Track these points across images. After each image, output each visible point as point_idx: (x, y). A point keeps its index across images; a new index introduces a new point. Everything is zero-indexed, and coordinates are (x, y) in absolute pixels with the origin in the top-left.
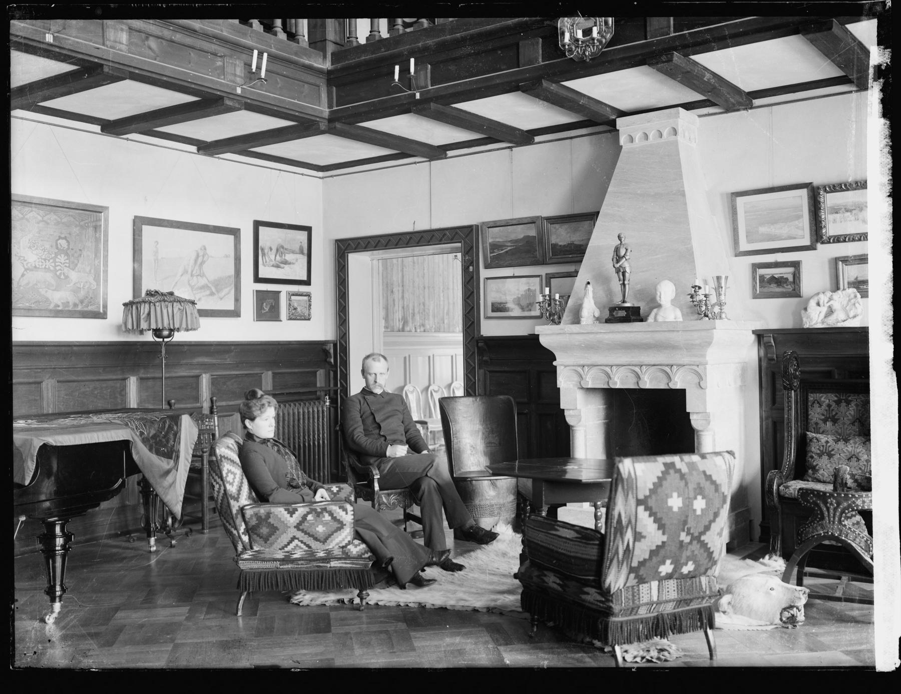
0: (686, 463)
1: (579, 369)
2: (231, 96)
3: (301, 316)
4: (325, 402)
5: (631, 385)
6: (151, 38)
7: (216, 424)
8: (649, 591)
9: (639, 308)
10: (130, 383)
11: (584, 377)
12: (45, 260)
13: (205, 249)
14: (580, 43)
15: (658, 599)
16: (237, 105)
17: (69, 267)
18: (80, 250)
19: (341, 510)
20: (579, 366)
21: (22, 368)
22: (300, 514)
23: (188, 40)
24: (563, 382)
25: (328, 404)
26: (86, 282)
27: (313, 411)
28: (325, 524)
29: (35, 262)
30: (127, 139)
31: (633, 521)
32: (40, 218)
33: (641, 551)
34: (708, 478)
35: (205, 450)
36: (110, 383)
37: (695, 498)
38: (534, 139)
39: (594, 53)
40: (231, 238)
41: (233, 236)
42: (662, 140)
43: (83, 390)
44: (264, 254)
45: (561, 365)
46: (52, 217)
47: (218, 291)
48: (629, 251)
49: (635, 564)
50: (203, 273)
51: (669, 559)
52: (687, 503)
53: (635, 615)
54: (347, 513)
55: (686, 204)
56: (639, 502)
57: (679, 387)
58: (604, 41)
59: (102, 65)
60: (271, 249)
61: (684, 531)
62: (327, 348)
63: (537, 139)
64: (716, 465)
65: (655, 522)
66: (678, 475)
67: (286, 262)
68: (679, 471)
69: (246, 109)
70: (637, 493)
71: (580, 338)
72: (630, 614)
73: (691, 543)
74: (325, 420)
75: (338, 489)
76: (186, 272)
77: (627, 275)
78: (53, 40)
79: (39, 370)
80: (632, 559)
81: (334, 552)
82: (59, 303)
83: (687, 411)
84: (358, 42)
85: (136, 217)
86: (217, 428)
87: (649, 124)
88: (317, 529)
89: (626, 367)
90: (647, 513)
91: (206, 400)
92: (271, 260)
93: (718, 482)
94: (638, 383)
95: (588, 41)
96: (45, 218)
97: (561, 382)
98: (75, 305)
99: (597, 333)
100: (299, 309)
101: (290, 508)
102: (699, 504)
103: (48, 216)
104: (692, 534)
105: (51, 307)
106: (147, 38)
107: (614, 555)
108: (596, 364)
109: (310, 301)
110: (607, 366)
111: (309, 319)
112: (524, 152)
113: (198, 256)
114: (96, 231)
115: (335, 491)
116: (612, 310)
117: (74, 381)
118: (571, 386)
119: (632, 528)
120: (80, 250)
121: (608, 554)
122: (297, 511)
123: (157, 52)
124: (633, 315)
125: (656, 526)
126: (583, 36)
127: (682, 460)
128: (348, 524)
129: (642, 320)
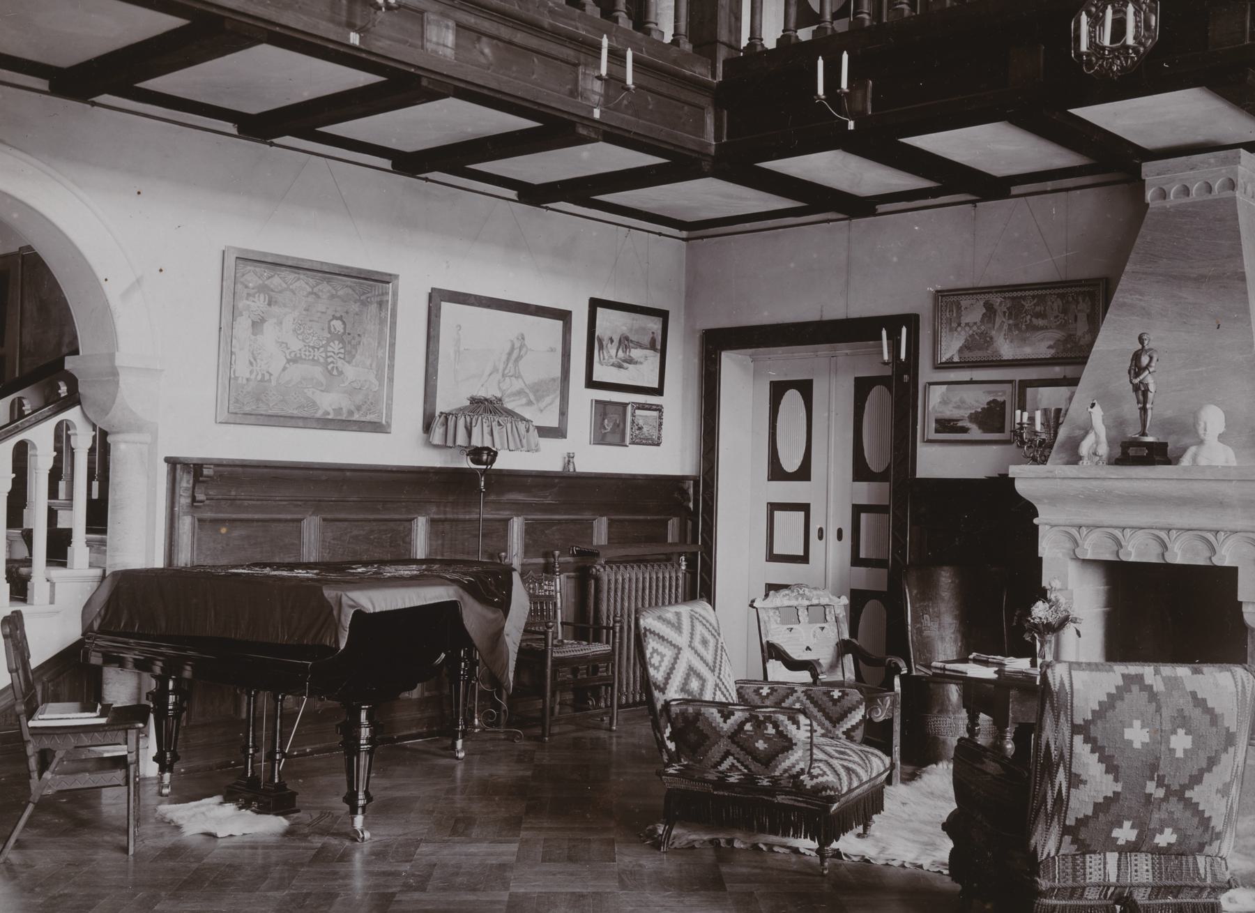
0: (1164, 679)
1: (1074, 531)
2: (586, 122)
3: (647, 439)
4: (680, 565)
5: (1153, 558)
6: (484, 39)
7: (558, 588)
8: (1102, 866)
9: (1166, 444)
10: (417, 526)
11: (1080, 542)
12: (313, 348)
13: (523, 339)
14: (1107, 53)
15: (1118, 880)
16: (593, 135)
17: (344, 359)
18: (359, 335)
19: (790, 722)
20: (1073, 526)
21: (277, 498)
22: (736, 721)
23: (534, 42)
24: (1047, 550)
25: (683, 568)
26: (365, 381)
27: (664, 578)
28: (767, 739)
29: (300, 350)
30: (427, 179)
31: (1067, 756)
32: (310, 290)
33: (1081, 804)
34: (1199, 702)
35: (551, 624)
36: (392, 524)
37: (1174, 732)
38: (1010, 191)
39: (1126, 67)
40: (559, 324)
41: (561, 322)
42: (1210, 197)
43: (355, 532)
44: (601, 347)
45: (1046, 524)
46: (325, 288)
47: (538, 401)
48: (1155, 359)
49: (1070, 822)
50: (519, 373)
51: (1128, 820)
52: (1159, 738)
53: (1079, 899)
54: (798, 728)
55: (1246, 293)
56: (1076, 729)
57: (1227, 563)
58: (1142, 49)
59: (419, 76)
60: (612, 340)
61: (1152, 779)
62: (686, 486)
63: (1015, 190)
64: (1217, 685)
65: (1100, 760)
66: (1145, 695)
67: (631, 361)
68: (1149, 688)
69: (606, 141)
70: (1072, 715)
71: (1078, 485)
72: (1071, 897)
73: (1166, 799)
74: (680, 590)
75: (840, 694)
76: (495, 370)
77: (1150, 395)
78: (360, 43)
79: (299, 503)
80: (1066, 813)
81: (782, 782)
82: (330, 410)
83: (1239, 599)
84: (762, 45)
85: (433, 289)
86: (558, 594)
87: (1192, 172)
88: (756, 745)
89: (1146, 531)
90: (1088, 747)
91: (517, 554)
92: (611, 357)
93: (1218, 711)
94: (1163, 555)
95: (1117, 49)
96: (316, 290)
97: (1044, 549)
98: (351, 413)
99: (1104, 479)
100: (645, 429)
101: (725, 709)
102: (1181, 742)
103: (320, 287)
104: (1168, 787)
105: (319, 414)
106: (479, 40)
107: (1041, 805)
108: (1101, 524)
109: (660, 417)
110: (1116, 527)
111: (658, 445)
112: (995, 210)
113: (513, 348)
114: (381, 309)
115: (836, 697)
116: (1126, 445)
117: (345, 520)
118: (1060, 555)
119: (1065, 767)
120: (359, 335)
121: (1033, 802)
122: (734, 715)
123: (491, 59)
124: (1158, 455)
125: (1102, 767)
126: (1111, 43)
127: (1157, 672)
128: (800, 744)
129: (1168, 462)
